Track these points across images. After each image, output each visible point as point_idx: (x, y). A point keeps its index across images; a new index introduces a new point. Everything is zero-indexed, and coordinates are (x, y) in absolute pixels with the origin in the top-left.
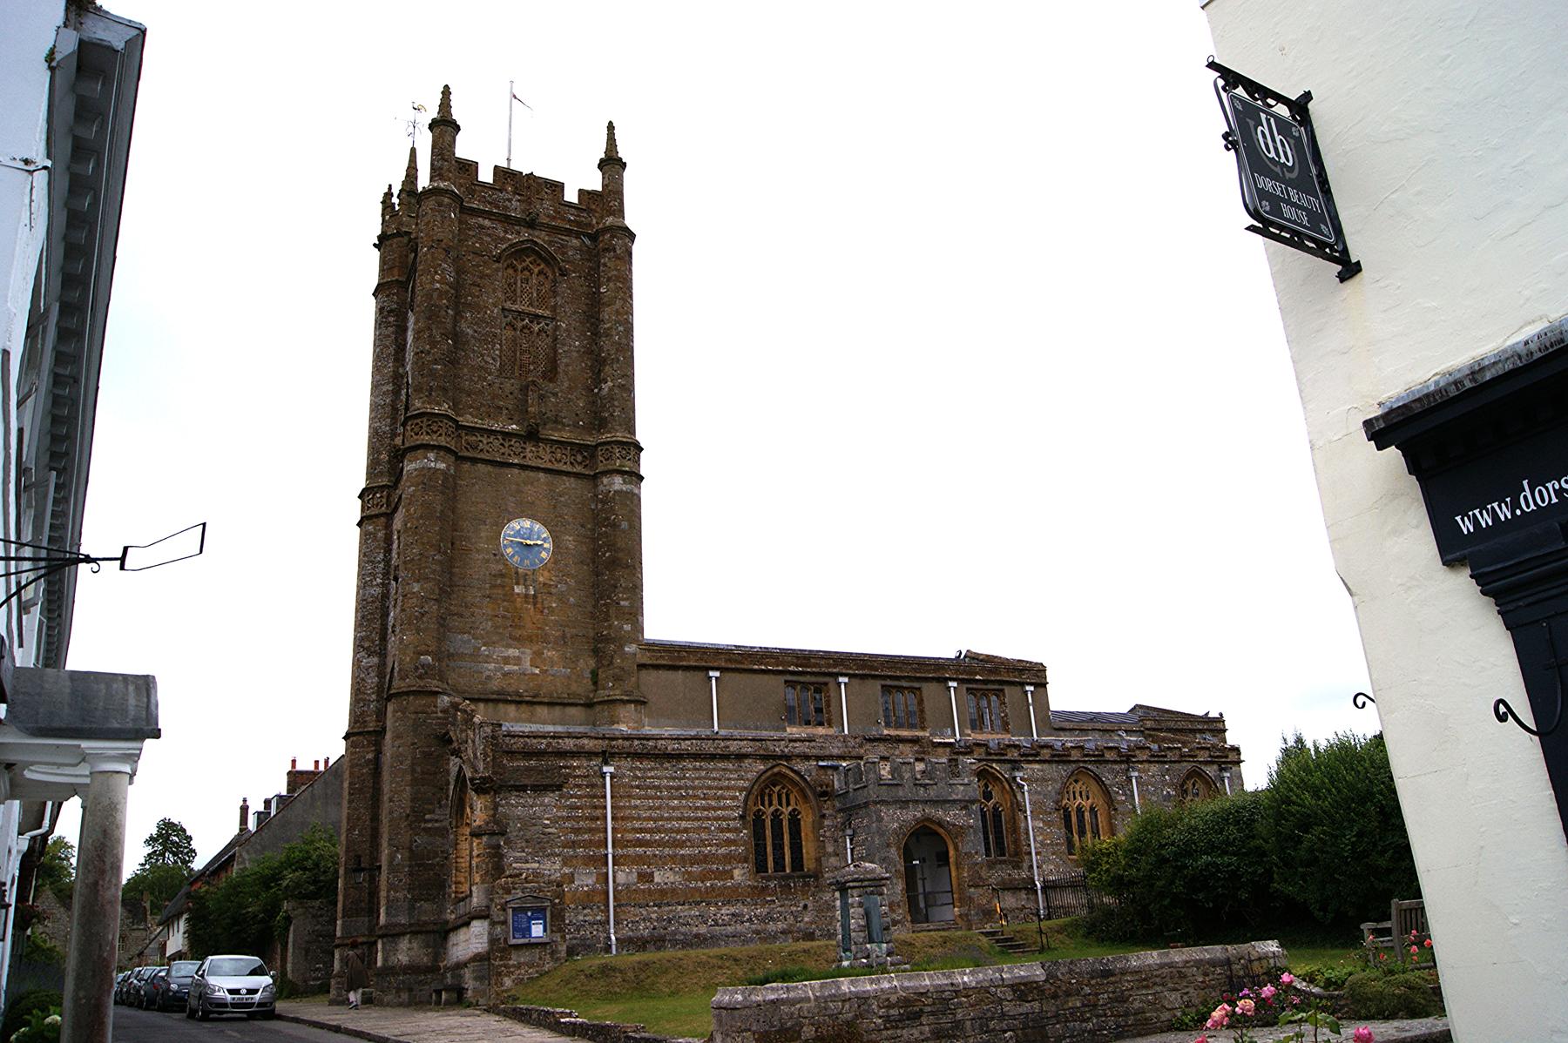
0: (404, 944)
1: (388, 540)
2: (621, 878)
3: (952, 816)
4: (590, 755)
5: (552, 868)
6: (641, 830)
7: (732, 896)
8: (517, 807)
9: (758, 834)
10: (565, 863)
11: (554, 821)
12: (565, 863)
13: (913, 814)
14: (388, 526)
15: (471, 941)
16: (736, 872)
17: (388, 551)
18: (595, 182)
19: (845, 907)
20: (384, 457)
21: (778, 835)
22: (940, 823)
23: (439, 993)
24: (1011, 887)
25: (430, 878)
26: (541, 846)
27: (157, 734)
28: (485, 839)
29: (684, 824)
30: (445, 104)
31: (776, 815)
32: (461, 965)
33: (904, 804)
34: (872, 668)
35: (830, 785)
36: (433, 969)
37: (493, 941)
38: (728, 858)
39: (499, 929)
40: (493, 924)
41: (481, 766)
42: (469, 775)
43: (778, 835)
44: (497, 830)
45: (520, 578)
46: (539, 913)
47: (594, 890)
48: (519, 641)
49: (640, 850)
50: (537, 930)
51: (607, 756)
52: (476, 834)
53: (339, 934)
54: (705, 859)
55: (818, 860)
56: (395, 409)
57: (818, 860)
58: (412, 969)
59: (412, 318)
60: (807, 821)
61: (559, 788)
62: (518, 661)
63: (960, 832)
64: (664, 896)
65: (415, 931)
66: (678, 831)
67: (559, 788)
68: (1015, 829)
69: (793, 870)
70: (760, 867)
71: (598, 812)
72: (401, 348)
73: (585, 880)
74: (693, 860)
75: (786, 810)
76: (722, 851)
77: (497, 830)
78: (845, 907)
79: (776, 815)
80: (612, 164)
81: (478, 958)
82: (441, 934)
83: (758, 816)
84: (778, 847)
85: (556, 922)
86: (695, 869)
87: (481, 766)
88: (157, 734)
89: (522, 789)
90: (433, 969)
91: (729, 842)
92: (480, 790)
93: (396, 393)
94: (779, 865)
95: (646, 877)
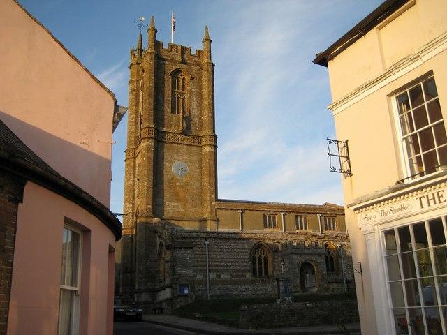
0: (143, 295)
1: (135, 166)
2: (211, 276)
3: (316, 259)
4: (201, 238)
5: (190, 273)
6: (218, 262)
7: (246, 283)
8: (180, 254)
9: (254, 264)
10: (194, 272)
11: (191, 258)
12: (194, 272)
13: (305, 258)
14: (135, 161)
15: (166, 294)
16: (247, 275)
17: (135, 170)
18: (201, 46)
19: (279, 286)
20: (133, 139)
21: (260, 264)
22: (312, 261)
23: (155, 310)
24: (336, 282)
25: (151, 275)
26: (186, 266)
27: (22, 202)
28: (169, 263)
29: (230, 260)
30: (153, 23)
31: (260, 258)
32: (161, 302)
33: (301, 255)
34: (299, 210)
35: (277, 248)
36: (153, 303)
37: (173, 294)
38: (244, 271)
39: (175, 291)
40: (173, 289)
41: (168, 242)
42: (164, 244)
43: (260, 264)
44: (173, 260)
45: (178, 180)
46: (187, 286)
47: (202, 280)
48: (178, 201)
49: (217, 268)
50: (186, 292)
51: (206, 239)
52: (166, 262)
53: (121, 291)
54: (238, 271)
55: (273, 272)
56: (136, 123)
57: (273, 272)
58: (146, 303)
59: (141, 93)
60: (270, 259)
61: (192, 248)
62: (177, 207)
63: (318, 264)
64: (224, 282)
65: (148, 291)
66: (229, 262)
67: (192, 248)
68: (338, 263)
69: (265, 274)
70: (254, 274)
71: (204, 256)
72: (165, 325)
73: (200, 277)
74: (233, 271)
75: (263, 257)
76: (243, 269)
77: (173, 260)
78: (279, 286)
79: (260, 258)
80: (208, 41)
81: (167, 299)
82: (154, 292)
83: (254, 258)
84: (260, 268)
85: (192, 288)
86: (234, 274)
87: (168, 242)
88: (22, 202)
89: (180, 248)
90: (153, 303)
91: (245, 266)
92: (168, 248)
93: (137, 117)
94: (261, 273)
95: (220, 276)
